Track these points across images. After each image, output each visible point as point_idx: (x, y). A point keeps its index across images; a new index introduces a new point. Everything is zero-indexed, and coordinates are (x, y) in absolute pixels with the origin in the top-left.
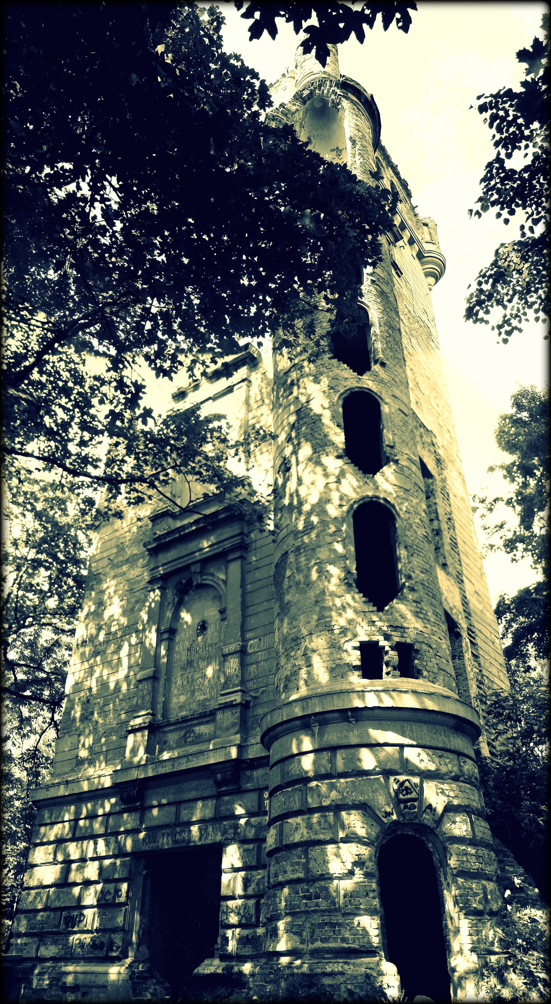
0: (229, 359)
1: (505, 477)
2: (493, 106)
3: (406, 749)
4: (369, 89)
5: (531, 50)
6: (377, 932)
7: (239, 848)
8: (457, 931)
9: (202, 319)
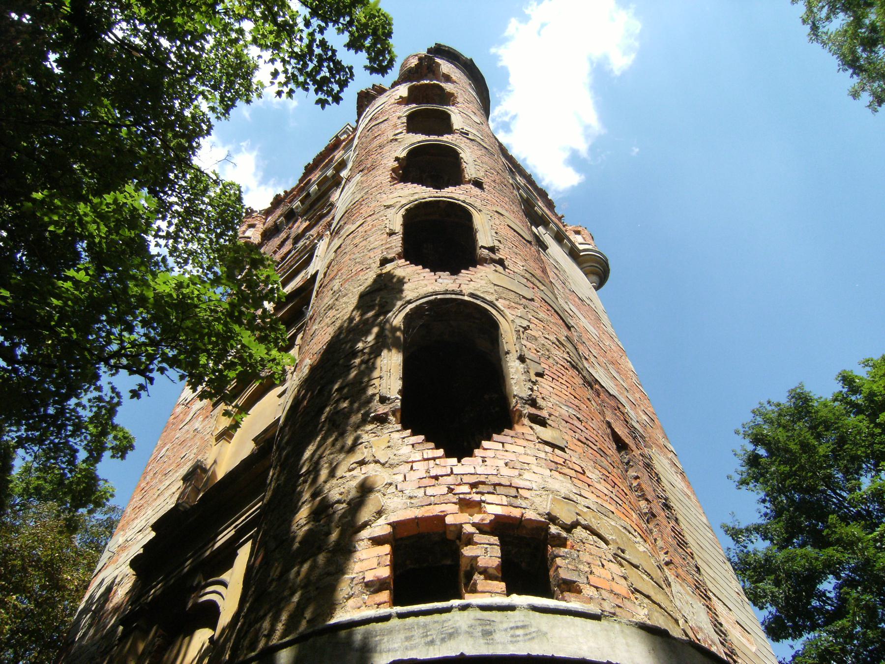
0: (312, 477)
1: (322, 103)
2: (374, 85)
3: (428, 489)
4: (467, 54)
5: (493, 50)
6: (467, 289)
7: (390, 350)
8: (471, 515)
9: (52, 196)
